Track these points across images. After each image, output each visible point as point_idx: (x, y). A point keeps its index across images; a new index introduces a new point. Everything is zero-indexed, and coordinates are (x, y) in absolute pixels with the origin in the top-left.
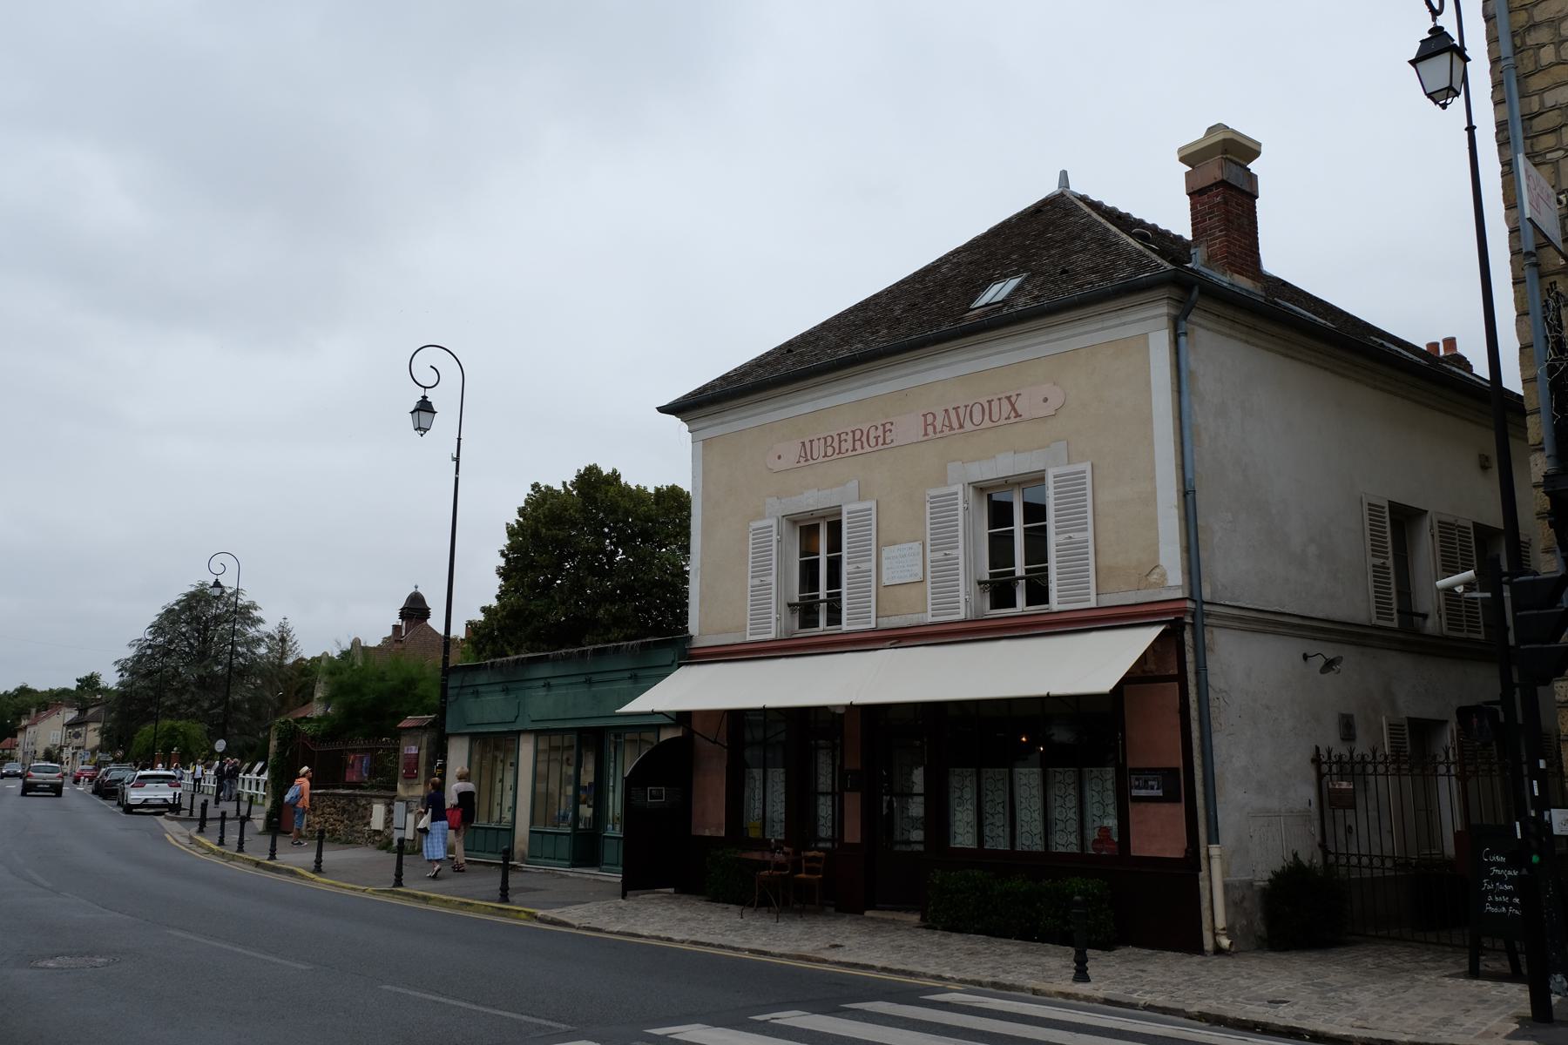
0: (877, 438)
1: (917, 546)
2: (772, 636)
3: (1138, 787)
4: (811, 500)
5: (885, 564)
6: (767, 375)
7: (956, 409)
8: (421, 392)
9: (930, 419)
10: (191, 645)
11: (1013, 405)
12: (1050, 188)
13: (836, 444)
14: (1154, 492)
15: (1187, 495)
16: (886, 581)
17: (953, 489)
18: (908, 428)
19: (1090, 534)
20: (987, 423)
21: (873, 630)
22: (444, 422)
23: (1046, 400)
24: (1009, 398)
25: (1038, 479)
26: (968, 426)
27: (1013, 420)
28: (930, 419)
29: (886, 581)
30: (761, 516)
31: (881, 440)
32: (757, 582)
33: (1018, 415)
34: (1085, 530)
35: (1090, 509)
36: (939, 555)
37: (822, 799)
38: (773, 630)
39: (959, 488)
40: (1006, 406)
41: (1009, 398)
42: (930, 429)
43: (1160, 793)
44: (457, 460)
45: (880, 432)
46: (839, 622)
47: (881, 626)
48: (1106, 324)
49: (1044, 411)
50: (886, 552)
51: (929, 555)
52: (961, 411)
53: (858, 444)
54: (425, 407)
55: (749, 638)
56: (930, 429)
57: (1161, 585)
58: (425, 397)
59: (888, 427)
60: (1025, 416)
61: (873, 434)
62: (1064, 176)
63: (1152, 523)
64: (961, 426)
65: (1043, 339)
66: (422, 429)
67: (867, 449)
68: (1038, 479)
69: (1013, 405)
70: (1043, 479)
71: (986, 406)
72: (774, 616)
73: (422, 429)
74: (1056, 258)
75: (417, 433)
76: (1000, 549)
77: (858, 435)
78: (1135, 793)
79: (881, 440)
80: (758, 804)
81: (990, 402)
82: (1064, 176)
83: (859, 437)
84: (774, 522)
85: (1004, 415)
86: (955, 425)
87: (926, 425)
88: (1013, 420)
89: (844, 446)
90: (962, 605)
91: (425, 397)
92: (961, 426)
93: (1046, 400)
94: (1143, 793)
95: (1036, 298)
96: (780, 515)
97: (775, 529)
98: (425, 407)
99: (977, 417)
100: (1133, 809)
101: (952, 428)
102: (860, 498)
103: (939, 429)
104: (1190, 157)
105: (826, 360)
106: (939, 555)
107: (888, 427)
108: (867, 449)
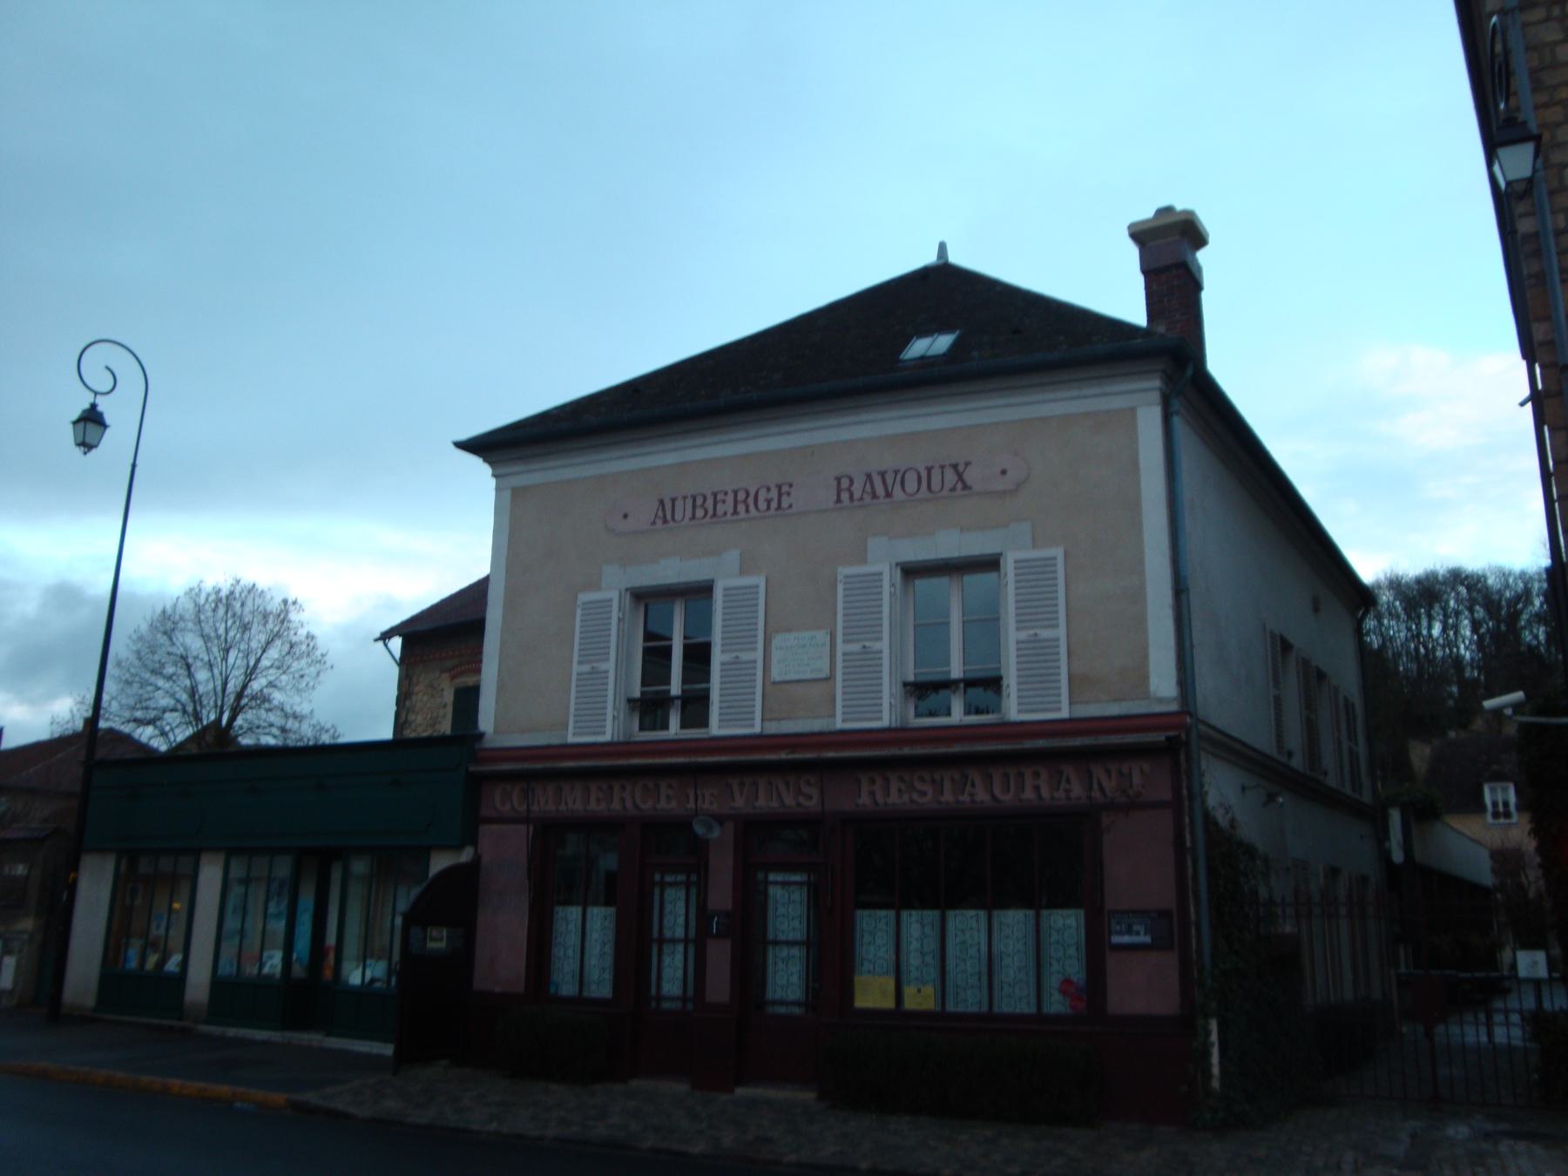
0: (769, 502)
1: (822, 636)
3: (1120, 933)
4: (670, 571)
5: (776, 655)
7: (883, 474)
8: (90, 398)
9: (845, 483)
10: (1417, 649)
12: (929, 258)
14: (1142, 587)
15: (1180, 590)
16: (776, 674)
19: (1061, 632)
22: (117, 439)
23: (1004, 472)
24: (955, 467)
25: (703, 591)
26: (898, 493)
29: (776, 674)
30: (594, 585)
31: (774, 505)
32: (586, 668)
33: (966, 487)
34: (880, 639)
36: (856, 647)
37: (679, 932)
38: (609, 729)
39: (885, 569)
40: (951, 477)
41: (955, 467)
42: (845, 496)
43: (1147, 939)
45: (774, 494)
46: (704, 723)
50: (777, 641)
51: (841, 648)
53: (741, 508)
54: (92, 420)
56: (845, 496)
57: (1146, 695)
58: (94, 406)
59: (785, 489)
61: (762, 495)
62: (942, 248)
63: (1140, 622)
64: (888, 495)
65: (1074, 393)
66: (86, 445)
68: (703, 591)
71: (924, 474)
72: (610, 712)
73: (86, 445)
74: (937, 336)
75: (78, 451)
76: (657, 655)
77: (741, 496)
78: (1116, 939)
79: (774, 505)
80: (573, 939)
81: (929, 470)
82: (942, 248)
83: (744, 500)
84: (614, 595)
86: (880, 491)
87: (839, 491)
88: (959, 491)
89: (721, 508)
91: (94, 406)
92: (888, 495)
93: (1004, 472)
94: (1126, 939)
96: (624, 586)
97: (615, 604)
98: (92, 420)
99: (911, 485)
100: (1112, 961)
101: (874, 496)
102: (743, 572)
103: (857, 495)
104: (1140, 235)
106: (856, 647)
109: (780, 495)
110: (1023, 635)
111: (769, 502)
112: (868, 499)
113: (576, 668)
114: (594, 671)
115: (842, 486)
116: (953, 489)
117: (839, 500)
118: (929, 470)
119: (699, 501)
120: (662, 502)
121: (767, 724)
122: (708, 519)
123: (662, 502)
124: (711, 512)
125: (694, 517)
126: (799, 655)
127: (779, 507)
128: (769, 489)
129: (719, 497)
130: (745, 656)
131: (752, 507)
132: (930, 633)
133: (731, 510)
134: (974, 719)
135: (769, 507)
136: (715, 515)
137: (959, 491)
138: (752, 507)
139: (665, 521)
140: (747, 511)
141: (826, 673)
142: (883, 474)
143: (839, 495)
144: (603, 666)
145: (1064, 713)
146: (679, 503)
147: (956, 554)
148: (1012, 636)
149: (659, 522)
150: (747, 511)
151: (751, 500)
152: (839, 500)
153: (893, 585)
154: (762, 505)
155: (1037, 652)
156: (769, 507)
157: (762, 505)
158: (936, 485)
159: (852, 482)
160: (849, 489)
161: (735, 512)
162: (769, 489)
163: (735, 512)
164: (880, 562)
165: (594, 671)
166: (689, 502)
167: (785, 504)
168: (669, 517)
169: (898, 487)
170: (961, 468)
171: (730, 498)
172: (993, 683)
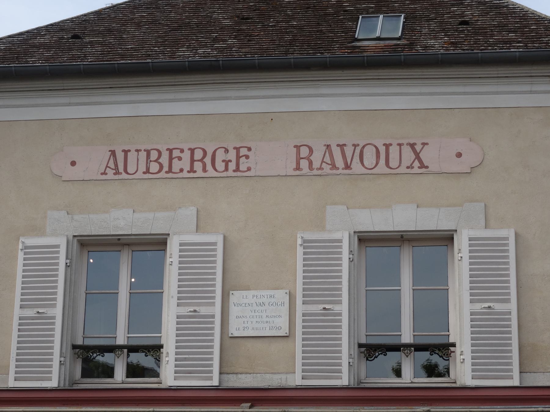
0: (227, 163)
1: (281, 296)
2: (53, 384)
4: (122, 220)
5: (234, 311)
6: (35, 61)
7: (342, 146)
9: (304, 152)
11: (417, 156)
13: (165, 160)
17: (336, 236)
18: (272, 157)
19: (513, 306)
20: (382, 168)
21: (216, 389)
23: (459, 155)
24: (412, 146)
26: (356, 167)
27: (416, 170)
28: (304, 152)
29: (234, 330)
31: (232, 166)
33: (422, 166)
34: (508, 301)
35: (513, 279)
36: (30, 313)
40: (408, 155)
42: (304, 164)
44: (138, 160)
45: (232, 155)
47: (225, 385)
48: (536, 88)
49: (462, 166)
50: (236, 297)
51: (300, 308)
52: (349, 151)
53: (198, 166)
55: (12, 384)
56: (304, 164)
59: (243, 152)
60: (433, 167)
61: (220, 156)
64: (347, 167)
65: (527, 88)
67: (211, 172)
69: (417, 156)
70: (451, 239)
71: (382, 150)
77: (198, 155)
79: (232, 166)
81: (387, 146)
84: (62, 242)
85: (406, 162)
86: (340, 163)
87: (299, 159)
90: (345, 368)
92: (347, 167)
95: (47, 60)
96: (71, 234)
101: (334, 166)
103: (316, 164)
105: (161, 59)
106: (30, 313)
107: (243, 152)
108: (214, 174)
109: (238, 157)
110: (185, 311)
111: (227, 163)
112: (327, 169)
113: (17, 312)
114: (40, 316)
115: (302, 155)
116: (411, 167)
117: (298, 168)
118: (387, 146)
119: (154, 155)
120: (113, 153)
121: (225, 377)
122: (162, 174)
123: (113, 153)
124: (166, 168)
125: (147, 171)
126: (259, 312)
127: (237, 169)
128: (227, 151)
129: (176, 153)
130: (203, 310)
131: (209, 167)
132: (378, 302)
133: (187, 168)
134: (425, 381)
135: (226, 169)
136: (170, 171)
137: (416, 170)
138: (209, 167)
139: (117, 173)
140: (205, 170)
141: (284, 331)
142: (342, 146)
143: (298, 163)
144: (50, 312)
145: (516, 382)
146: (132, 156)
147: (412, 228)
148: (170, 312)
149: (110, 172)
150: (205, 170)
151: (208, 160)
152: (298, 168)
153: (351, 252)
154: (220, 166)
155: (486, 327)
156: (226, 169)
157: (220, 166)
158: (394, 163)
159: (311, 150)
160: (308, 158)
161: (192, 170)
162: (227, 151)
163: (192, 170)
164: (342, 225)
165: (40, 316)
166: (143, 155)
167: (243, 167)
168: (121, 169)
169: (357, 159)
170: (418, 148)
171: (186, 156)
172: (445, 349)
